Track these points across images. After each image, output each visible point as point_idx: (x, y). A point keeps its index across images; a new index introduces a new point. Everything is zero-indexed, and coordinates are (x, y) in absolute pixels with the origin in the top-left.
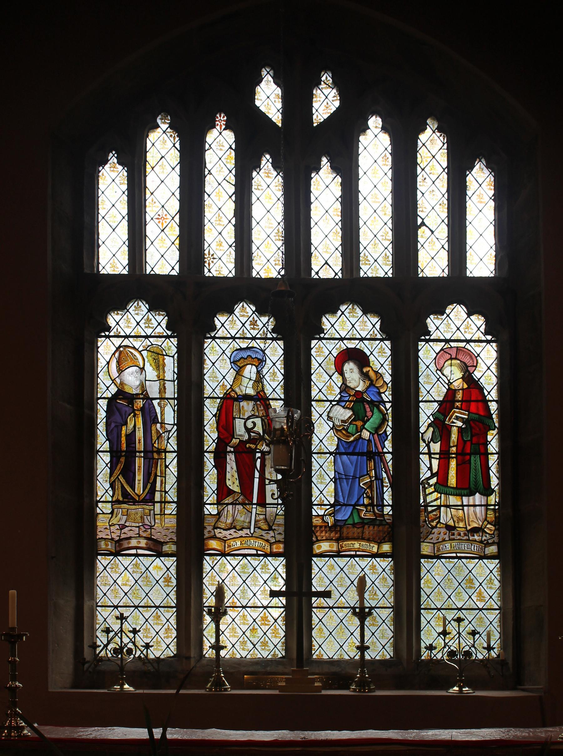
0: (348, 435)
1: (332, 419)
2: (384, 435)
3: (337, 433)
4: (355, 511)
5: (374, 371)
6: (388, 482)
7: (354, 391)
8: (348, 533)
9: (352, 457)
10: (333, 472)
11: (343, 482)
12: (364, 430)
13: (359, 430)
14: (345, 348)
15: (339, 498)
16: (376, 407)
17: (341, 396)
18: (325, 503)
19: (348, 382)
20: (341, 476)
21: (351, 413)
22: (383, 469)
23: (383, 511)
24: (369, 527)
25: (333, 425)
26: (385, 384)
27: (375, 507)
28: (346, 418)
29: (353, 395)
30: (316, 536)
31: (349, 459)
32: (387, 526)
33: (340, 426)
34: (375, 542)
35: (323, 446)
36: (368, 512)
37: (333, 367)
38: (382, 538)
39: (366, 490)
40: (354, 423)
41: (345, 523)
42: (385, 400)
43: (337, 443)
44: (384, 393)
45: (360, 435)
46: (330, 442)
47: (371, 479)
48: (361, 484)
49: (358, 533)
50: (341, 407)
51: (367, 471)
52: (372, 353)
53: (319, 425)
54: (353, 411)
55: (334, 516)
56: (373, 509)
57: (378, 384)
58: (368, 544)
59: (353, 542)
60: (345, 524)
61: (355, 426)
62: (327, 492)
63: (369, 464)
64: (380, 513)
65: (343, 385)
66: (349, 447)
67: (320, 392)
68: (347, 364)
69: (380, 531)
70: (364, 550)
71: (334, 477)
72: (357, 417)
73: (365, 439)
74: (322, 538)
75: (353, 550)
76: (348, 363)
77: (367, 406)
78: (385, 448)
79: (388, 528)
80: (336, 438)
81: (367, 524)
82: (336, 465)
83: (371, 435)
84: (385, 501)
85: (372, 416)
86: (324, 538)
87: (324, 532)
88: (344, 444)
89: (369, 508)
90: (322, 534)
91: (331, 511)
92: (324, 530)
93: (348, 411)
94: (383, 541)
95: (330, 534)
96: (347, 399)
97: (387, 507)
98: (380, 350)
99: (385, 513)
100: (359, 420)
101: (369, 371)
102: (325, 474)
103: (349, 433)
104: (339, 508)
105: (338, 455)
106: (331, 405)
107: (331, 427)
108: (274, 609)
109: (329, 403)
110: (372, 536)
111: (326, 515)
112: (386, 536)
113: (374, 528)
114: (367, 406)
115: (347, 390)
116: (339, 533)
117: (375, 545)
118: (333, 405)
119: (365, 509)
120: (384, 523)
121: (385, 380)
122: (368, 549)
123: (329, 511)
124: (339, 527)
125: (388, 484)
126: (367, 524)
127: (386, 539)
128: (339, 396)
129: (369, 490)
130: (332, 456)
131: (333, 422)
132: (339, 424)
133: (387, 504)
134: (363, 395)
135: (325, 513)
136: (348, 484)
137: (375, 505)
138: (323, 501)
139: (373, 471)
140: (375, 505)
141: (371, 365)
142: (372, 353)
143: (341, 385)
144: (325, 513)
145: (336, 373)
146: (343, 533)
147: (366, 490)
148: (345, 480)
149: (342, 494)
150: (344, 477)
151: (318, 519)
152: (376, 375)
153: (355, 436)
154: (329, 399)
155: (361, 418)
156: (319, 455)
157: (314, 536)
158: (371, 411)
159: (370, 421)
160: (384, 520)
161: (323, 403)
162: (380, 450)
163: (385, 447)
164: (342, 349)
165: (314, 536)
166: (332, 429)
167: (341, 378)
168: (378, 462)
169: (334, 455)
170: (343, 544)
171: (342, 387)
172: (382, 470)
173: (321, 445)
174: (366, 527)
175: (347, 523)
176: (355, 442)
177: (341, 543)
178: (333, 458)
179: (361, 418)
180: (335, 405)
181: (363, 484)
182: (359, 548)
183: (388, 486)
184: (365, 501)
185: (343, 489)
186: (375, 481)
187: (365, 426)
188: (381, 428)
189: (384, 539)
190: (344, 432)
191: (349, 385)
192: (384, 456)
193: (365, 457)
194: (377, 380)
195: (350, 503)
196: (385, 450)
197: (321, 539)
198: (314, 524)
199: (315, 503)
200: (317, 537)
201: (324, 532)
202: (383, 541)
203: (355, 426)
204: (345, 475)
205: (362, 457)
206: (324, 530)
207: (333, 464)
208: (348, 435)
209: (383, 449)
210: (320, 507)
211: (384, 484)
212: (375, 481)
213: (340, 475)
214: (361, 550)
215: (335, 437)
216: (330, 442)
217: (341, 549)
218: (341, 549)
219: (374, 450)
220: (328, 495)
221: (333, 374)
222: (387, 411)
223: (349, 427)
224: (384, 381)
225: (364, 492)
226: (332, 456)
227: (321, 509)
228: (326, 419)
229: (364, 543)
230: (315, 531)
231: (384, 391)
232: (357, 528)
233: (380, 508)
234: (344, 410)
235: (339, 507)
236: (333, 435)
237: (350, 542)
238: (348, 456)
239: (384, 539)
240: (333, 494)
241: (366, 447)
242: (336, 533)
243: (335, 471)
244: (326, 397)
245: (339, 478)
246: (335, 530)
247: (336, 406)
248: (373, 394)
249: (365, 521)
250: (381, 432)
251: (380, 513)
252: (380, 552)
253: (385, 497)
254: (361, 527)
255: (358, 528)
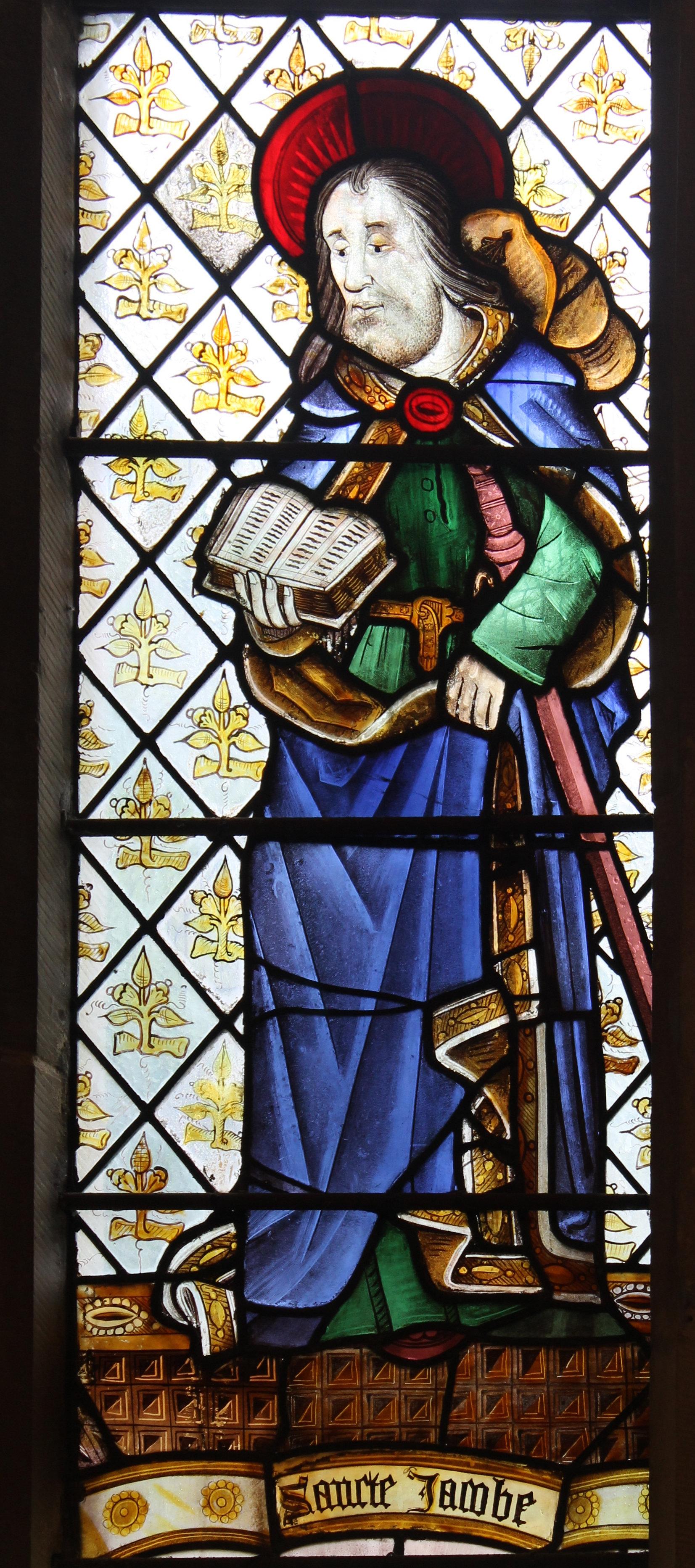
0: (350, 696)
1: (232, 586)
2: (609, 700)
3: (267, 683)
4: (394, 1242)
5: (545, 239)
6: (636, 1034)
7: (398, 385)
8: (339, 1406)
9: (372, 856)
10: (240, 967)
11: (311, 1041)
12: (468, 668)
13: (429, 665)
14: (334, 68)
15: (275, 1149)
16: (556, 500)
17: (303, 419)
18: (171, 1188)
19: (353, 316)
20: (293, 995)
21: (372, 539)
22: (605, 944)
23: (597, 1244)
24: (493, 1359)
25: (240, 626)
26: (620, 330)
27: (543, 1217)
28: (334, 576)
29: (386, 416)
30: (101, 1425)
31: (354, 876)
32: (623, 1354)
33: (289, 633)
34: (537, 1465)
35: (163, 783)
36: (485, 1247)
37: (245, 205)
38: (587, 1437)
39: (473, 1090)
40: (395, 612)
41: (321, 1330)
42: (618, 445)
43: (264, 755)
44: (613, 395)
45: (441, 696)
46: (212, 752)
47: (511, 1012)
48: (441, 1053)
49: (418, 1404)
50: (299, 501)
51: (488, 959)
52: (527, 109)
53: (133, 627)
54: (386, 526)
55: (237, 1285)
56: (529, 1228)
57: (572, 331)
58: (491, 1484)
59: (381, 1472)
60: (317, 1343)
61: (399, 634)
62: (189, 1110)
63: (504, 909)
64: (573, 1255)
65: (318, 341)
66: (356, 786)
67: (146, 393)
68: (345, 187)
69: (571, 1386)
70: (460, 1528)
71: (244, 1006)
72: (413, 568)
73: (472, 729)
74: (150, 1440)
75: (379, 1525)
76: (359, 184)
77: (491, 493)
78: (618, 795)
79: (634, 1367)
80: (258, 721)
81: (480, 1334)
82: (260, 918)
83: (518, 703)
84: (612, 1174)
85: (525, 564)
86: (164, 1444)
87: (162, 1401)
88: (320, 761)
89: (496, 1220)
90: (148, 1417)
91: (214, 1244)
92: (166, 1385)
93: (345, 525)
94: (596, 1459)
95: (210, 1415)
96: (343, 436)
97: (629, 1215)
98: (588, 91)
99: (616, 1254)
100: (430, 590)
101: (508, 236)
102: (179, 980)
103: (356, 683)
104: (282, 1225)
105: (274, 847)
106: (226, 484)
107: (227, 638)
108: (525, 385)
109: (205, 468)
110: (516, 1421)
111: (177, 1278)
112: (615, 1425)
113: (528, 1365)
114: (491, 493)
115: (342, 375)
116: (273, 1405)
117: (539, 1493)
118: (242, 485)
119: (466, 1231)
120: (606, 1328)
121: (620, 302)
122: (488, 1517)
123: (202, 1250)
124: (272, 1365)
125: (641, 1052)
126: (480, 1334)
127: (621, 1443)
128: (285, 418)
129: (501, 1091)
130: (226, 851)
131: (235, 604)
132: (278, 621)
133: (625, 1188)
134: (459, 411)
135: (174, 1265)
136: (342, 1052)
137: (543, 1202)
138: (162, 1175)
139: (532, 954)
140: (543, 1202)
141: (522, 193)
142: (527, 109)
143: (304, 342)
144: (174, 1265)
145: (269, 251)
146: (302, 1404)
147: (473, 1090)
148: (322, 1026)
149: (303, 1128)
150: (315, 998)
151: (120, 1303)
152: (558, 266)
153: (398, 707)
154: (210, 435)
155: (443, 577)
156: (134, 843)
157: (90, 1431)
158: (518, 524)
159: (513, 598)
160: (609, 1305)
161: (163, 464)
162: (586, 804)
163: (615, 782)
164: (307, 82)
165: (90, 1431)
166: (224, 653)
167: (304, 288)
168: (566, 891)
169: (242, 841)
170: (303, 1485)
171: (310, 353)
172: (595, 950)
173: (145, 775)
174: (474, 1355)
175: (333, 1331)
176: (400, 752)
177: (293, 1479)
178: (235, 864)
179: (443, 577)
180: (254, 481)
181: (455, 1053)
182: (422, 1514)
183: (635, 1061)
184: (467, 1171)
185: (307, 1084)
186: (541, 1031)
187: (479, 637)
188: (592, 646)
189: (603, 1442)
190: (317, 677)
191: (359, 337)
192: (610, 846)
193: (471, 861)
194: (561, 304)
195: (355, 1186)
196: (618, 805)
197: (139, 1448)
198: (86, 1344)
199: (101, 1185)
200: (108, 1439)
201: (162, 1401)
202: (596, 1459)
203: (399, 634)
204: (326, 989)
205: (450, 859)
206: (166, 1385)
207: (235, 907)
208: (350, 696)
209: (601, 799)
210: (130, 1215)
211: (608, 1050)
212: (541, 1031)
213: (282, 985)
214: (434, 1527)
215: (254, 712)
216: (212, 752)
217: (290, 1519)
218: (290, 1519)
219: (534, 803)
220: (195, 1133)
221: (247, 259)
222: (634, 531)
223: (354, 642)
224: (617, 314)
225: (463, 1112)
226: (226, 851)
227: (143, 1233)
228: (185, 587)
229: (460, 1478)
230: (97, 1396)
231: (616, 378)
232: (401, 1363)
233: (576, 1218)
234: (317, 516)
235: (275, 1217)
236: (239, 698)
237: (353, 1474)
238: (350, 851)
239: (603, 1442)
240: (237, 1126)
241: (476, 783)
242: (253, 1407)
243: (252, 962)
244: (172, 464)
245: (283, 1012)
246: (243, 1386)
247: (263, 489)
248: (534, 406)
249: (469, 1319)
250: (592, 679)
251: (573, 1255)
252: (573, 1539)
253: (610, 1144)
254: (433, 1362)
255: (415, 1367)
